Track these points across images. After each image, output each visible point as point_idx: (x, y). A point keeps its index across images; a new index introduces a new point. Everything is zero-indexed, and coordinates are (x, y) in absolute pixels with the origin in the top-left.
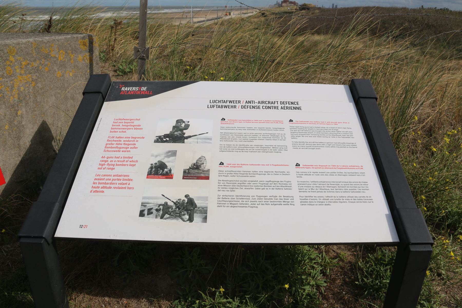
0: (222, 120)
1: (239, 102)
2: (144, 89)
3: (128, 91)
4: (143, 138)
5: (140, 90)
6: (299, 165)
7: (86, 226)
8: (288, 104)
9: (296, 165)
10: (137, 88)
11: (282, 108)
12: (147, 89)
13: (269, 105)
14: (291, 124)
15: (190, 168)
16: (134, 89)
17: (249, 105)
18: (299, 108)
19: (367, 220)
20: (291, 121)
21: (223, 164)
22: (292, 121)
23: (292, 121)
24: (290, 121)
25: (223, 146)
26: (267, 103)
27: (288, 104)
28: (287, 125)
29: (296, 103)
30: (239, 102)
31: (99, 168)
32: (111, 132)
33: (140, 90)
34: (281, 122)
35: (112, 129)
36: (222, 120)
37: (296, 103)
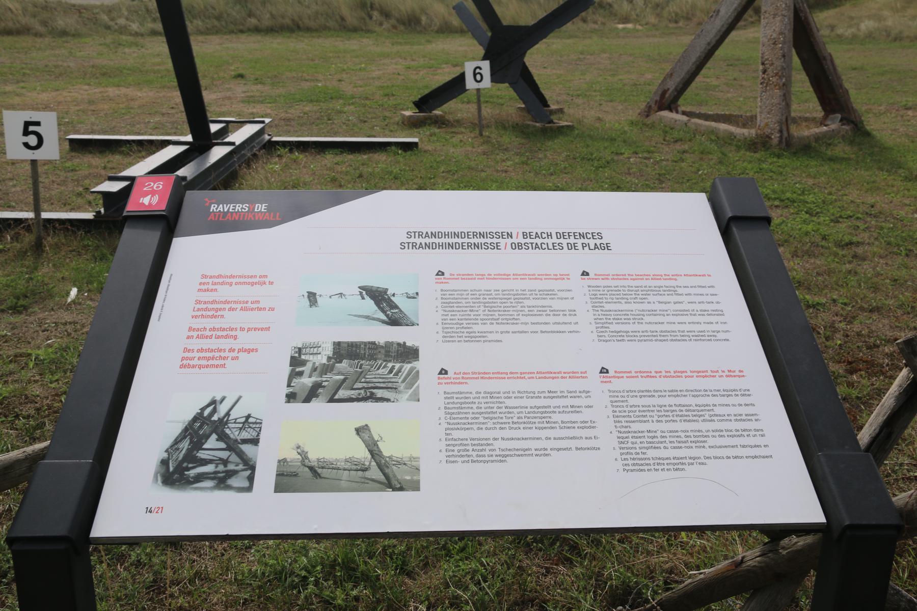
0: (437, 275)
1: (510, 235)
2: (261, 208)
3: (225, 214)
4: (268, 329)
5: (251, 210)
6: (607, 372)
7: (160, 509)
8: (572, 238)
9: (601, 372)
10: (246, 207)
11: (596, 247)
12: (269, 209)
13: (476, 240)
14: (587, 282)
15: (74, 6)
16: (239, 207)
17: (532, 241)
18: (607, 247)
19: (785, 494)
20: (585, 274)
21: (446, 373)
22: (588, 274)
23: (588, 274)
24: (583, 274)
25: (659, 434)
26: (544, 236)
27: (572, 238)
28: (578, 286)
29: (589, 236)
30: (510, 235)
31: (188, 337)
32: (200, 290)
33: (251, 210)
34: (583, 375)
35: (200, 284)
36: (437, 275)
37: (589, 236)
